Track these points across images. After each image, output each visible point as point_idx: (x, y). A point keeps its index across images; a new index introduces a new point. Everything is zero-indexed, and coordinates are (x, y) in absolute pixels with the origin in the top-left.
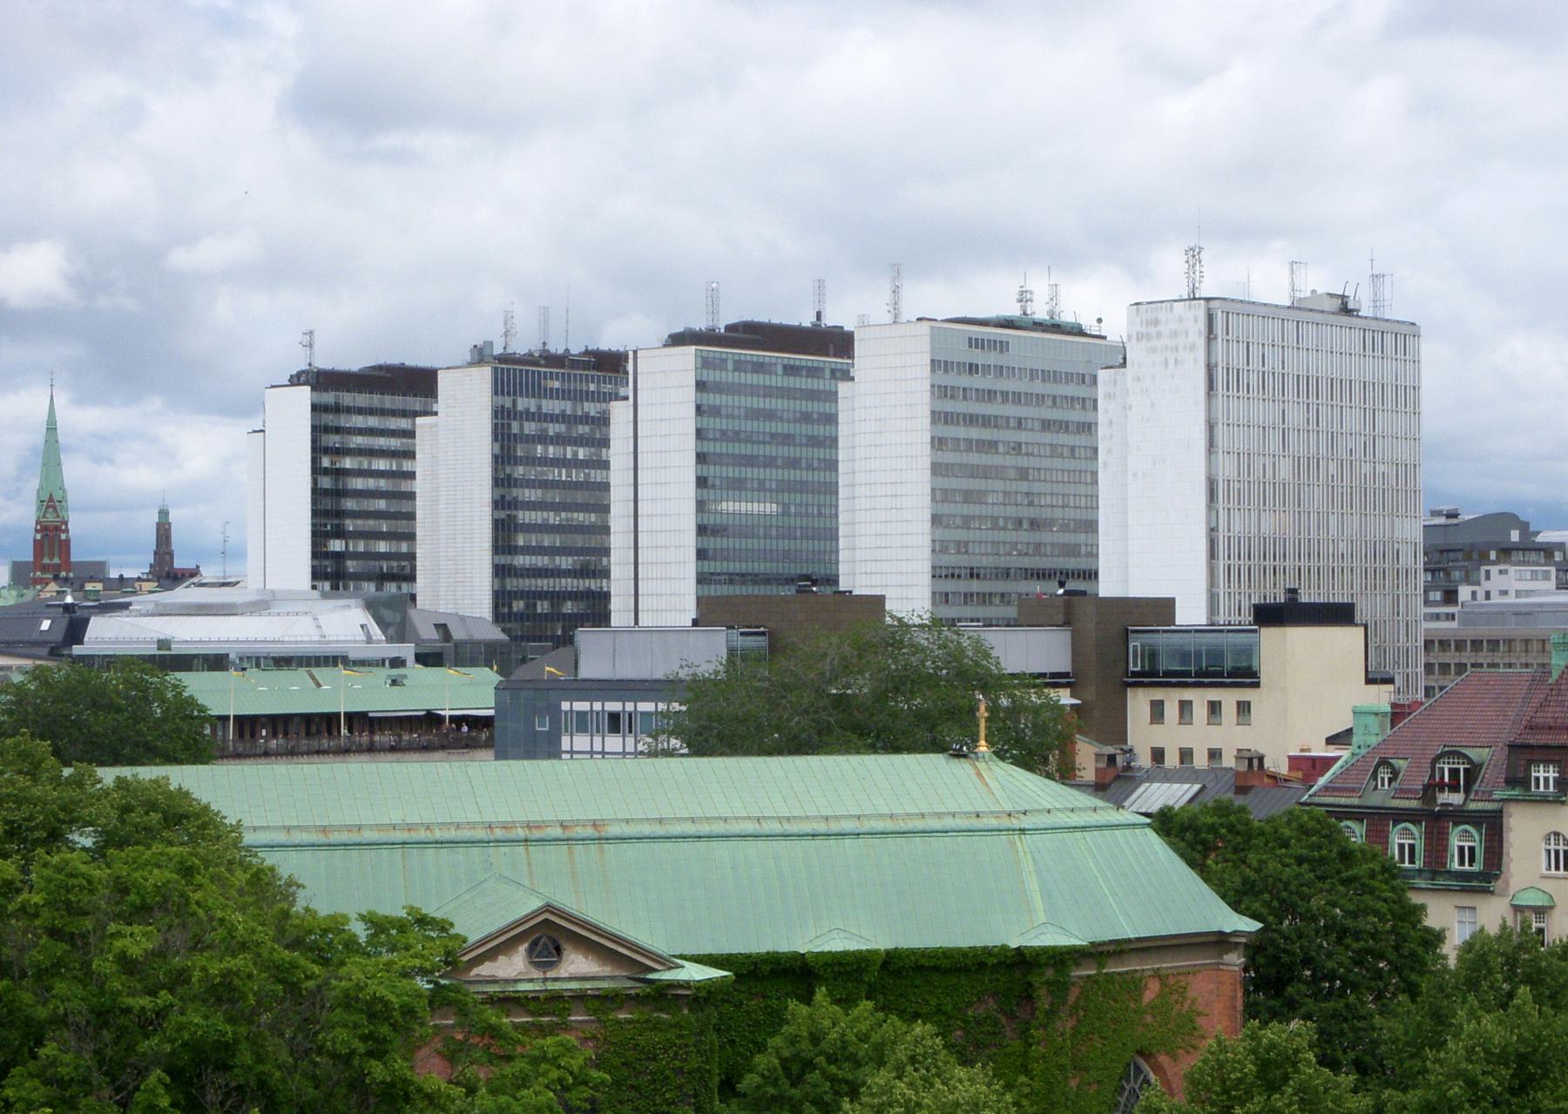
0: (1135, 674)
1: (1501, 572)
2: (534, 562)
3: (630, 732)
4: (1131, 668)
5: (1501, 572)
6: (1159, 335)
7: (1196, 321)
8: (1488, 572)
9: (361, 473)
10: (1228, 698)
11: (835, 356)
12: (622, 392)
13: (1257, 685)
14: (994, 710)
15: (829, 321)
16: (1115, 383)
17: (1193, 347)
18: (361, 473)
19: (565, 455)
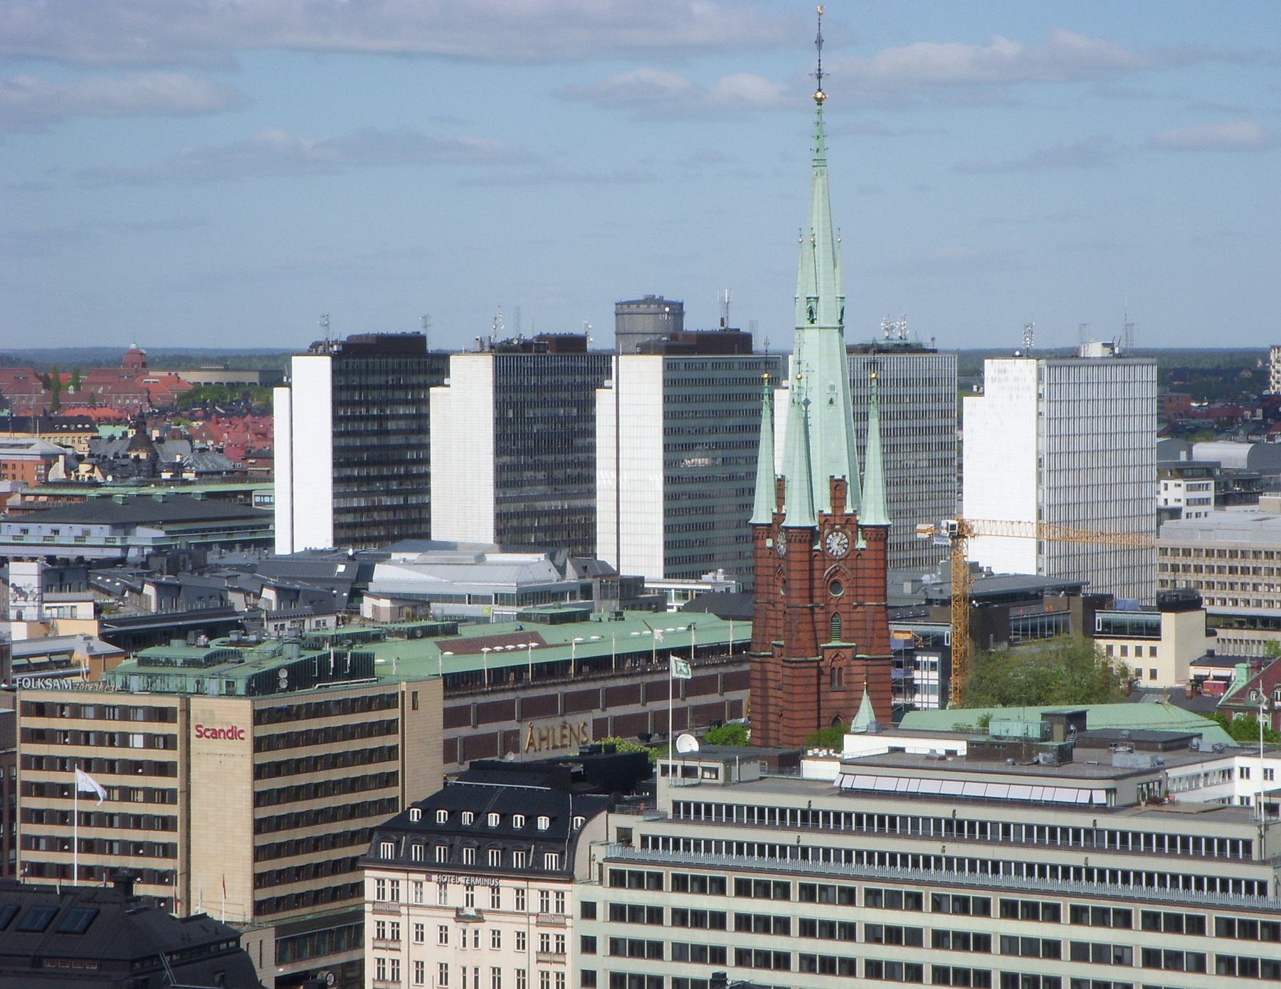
0: (1098, 633)
1: (1176, 485)
2: (420, 498)
3: (364, 667)
4: (1097, 629)
5: (1176, 485)
6: (1006, 379)
7: (1031, 372)
8: (1166, 485)
9: (368, 433)
10: (1146, 645)
11: (739, 353)
12: (606, 383)
13: (1160, 640)
14: (728, 654)
15: (732, 324)
16: (975, 405)
17: (1029, 388)
18: (368, 433)
19: (387, 382)
